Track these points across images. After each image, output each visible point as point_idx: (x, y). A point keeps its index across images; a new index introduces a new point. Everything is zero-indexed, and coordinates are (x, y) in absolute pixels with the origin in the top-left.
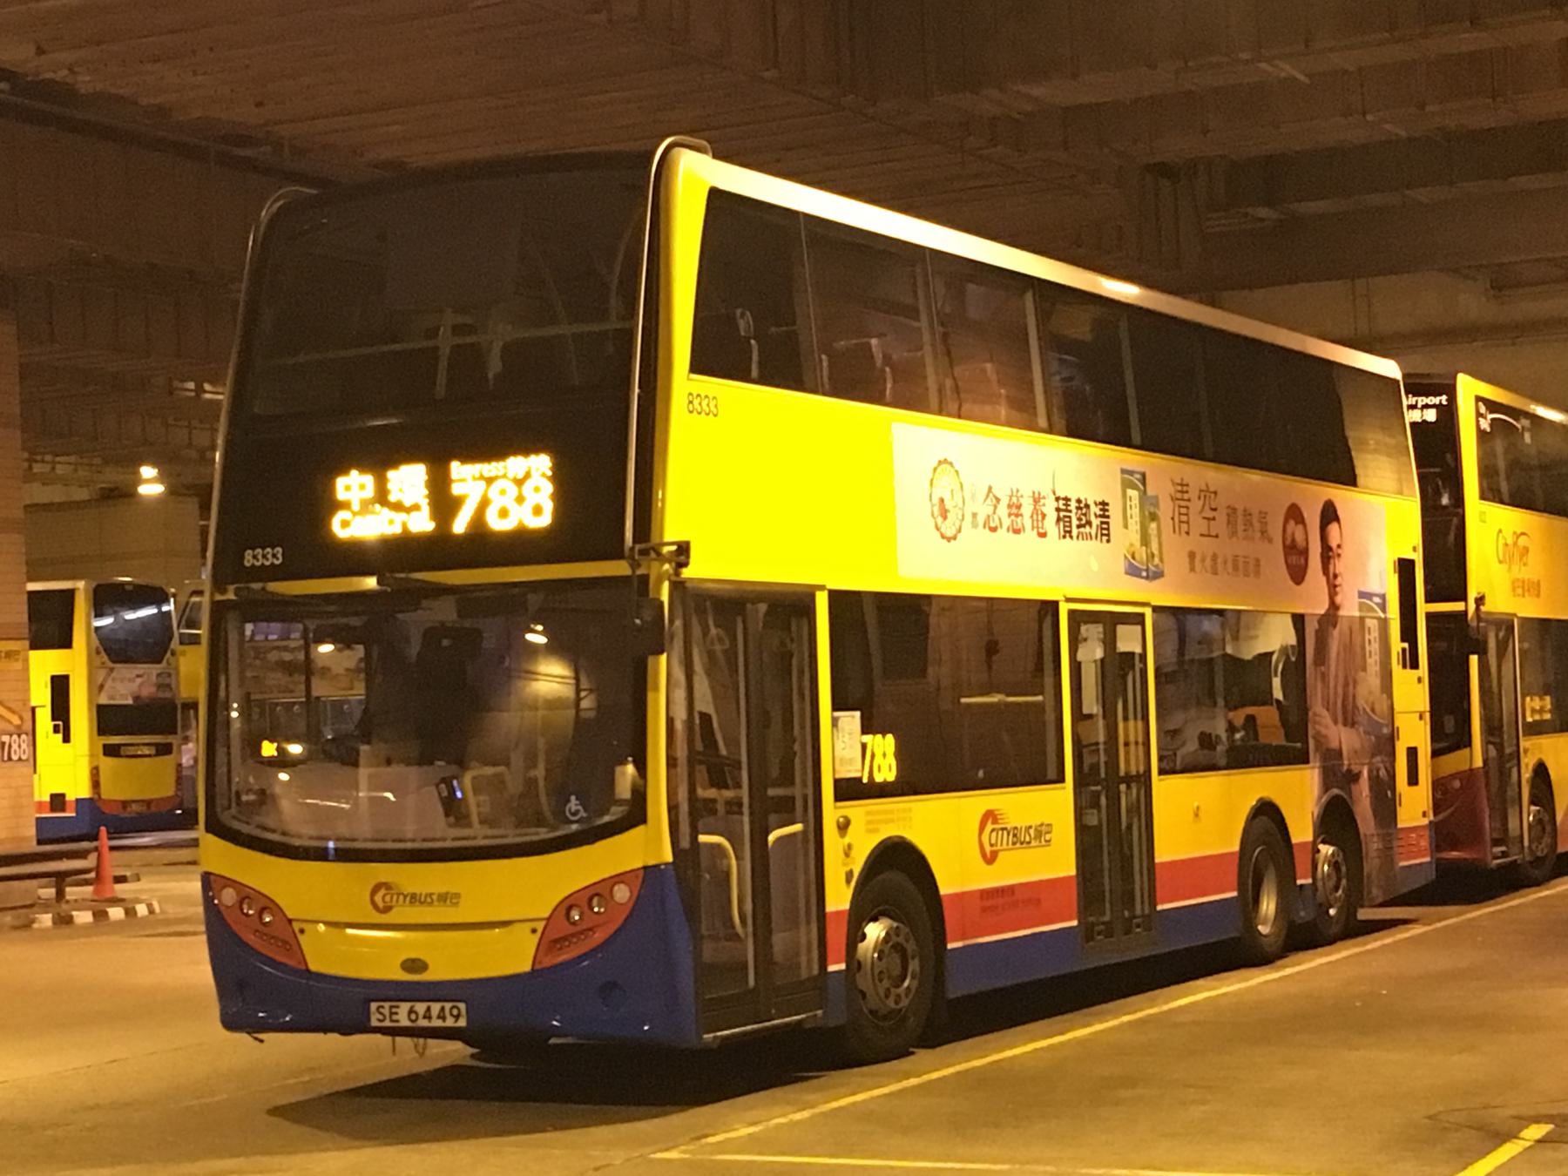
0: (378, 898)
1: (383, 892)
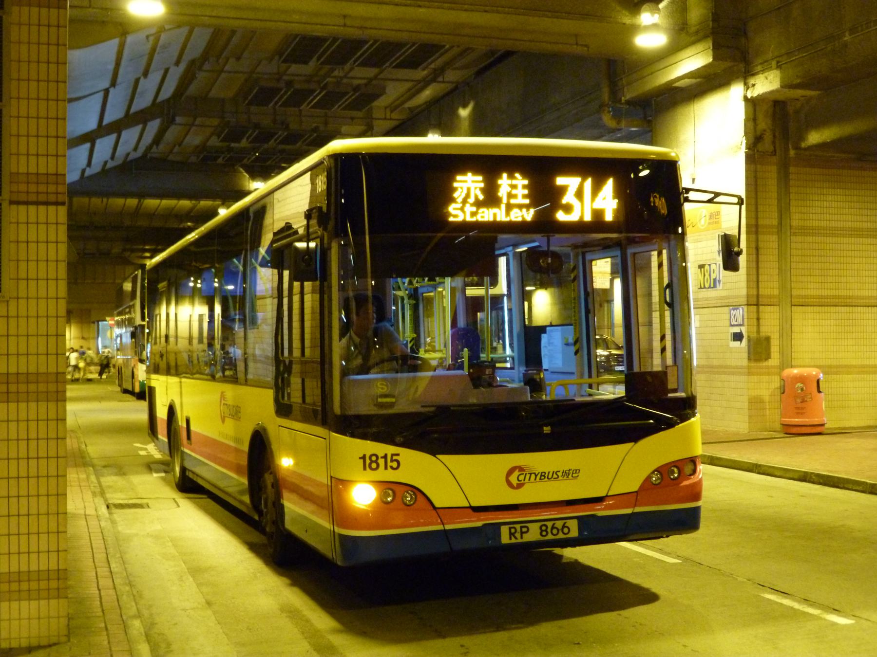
0: (513, 479)
1: (517, 473)
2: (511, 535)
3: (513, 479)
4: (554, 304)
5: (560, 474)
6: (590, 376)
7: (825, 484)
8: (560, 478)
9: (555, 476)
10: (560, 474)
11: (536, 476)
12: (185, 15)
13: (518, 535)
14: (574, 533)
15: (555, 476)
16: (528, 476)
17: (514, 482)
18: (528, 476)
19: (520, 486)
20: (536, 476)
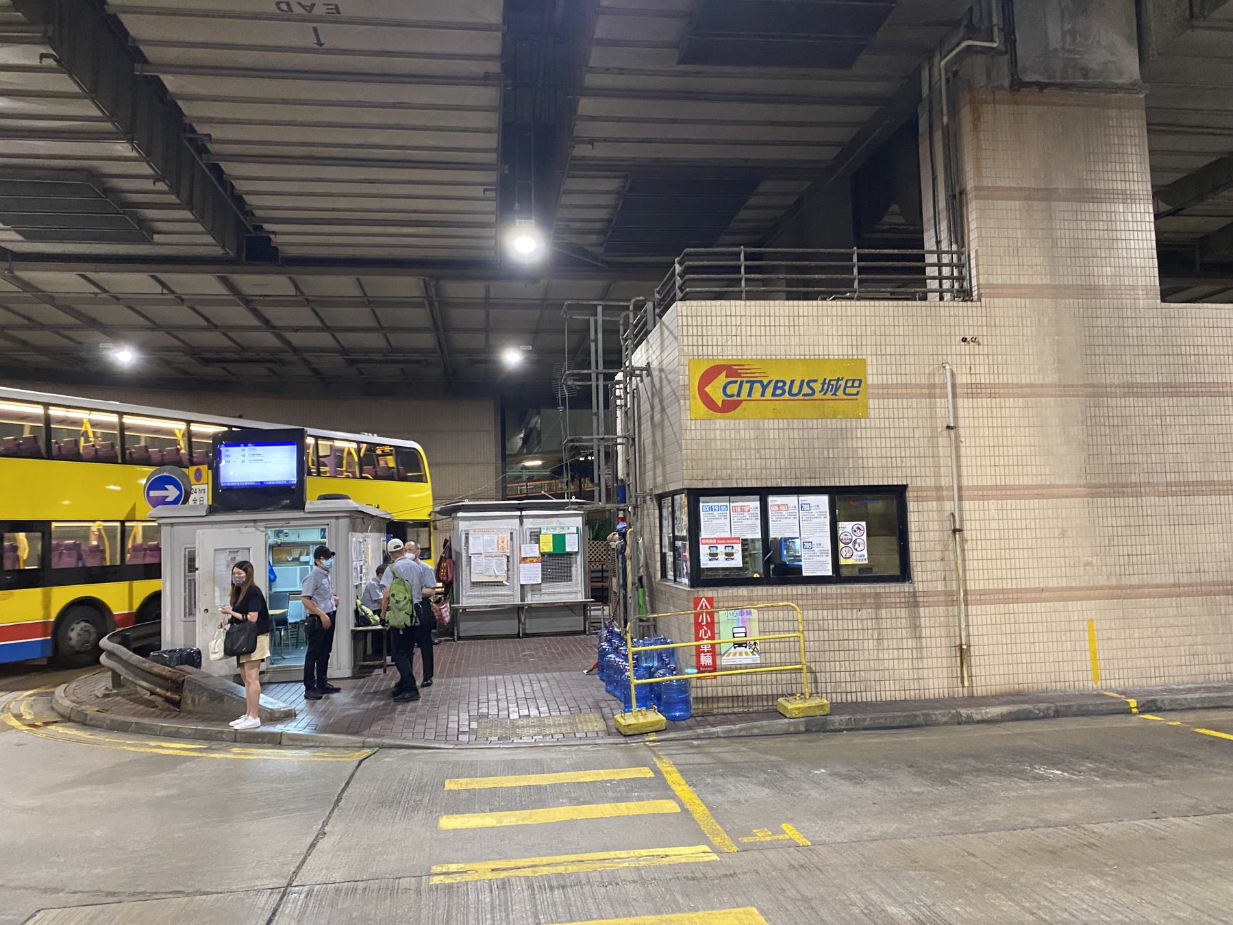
0: (715, 391)
1: (722, 379)
2: (713, 556)
3: (715, 391)
4: (112, 364)
5: (817, 386)
6: (749, 270)
7: (460, 28)
8: (818, 395)
9: (806, 390)
10: (817, 386)
11: (764, 388)
12: (480, 238)
13: (722, 557)
14: (802, 728)
15: (806, 390)
16: (746, 387)
17: (718, 397)
18: (746, 387)
19: (730, 406)
20: (764, 388)
